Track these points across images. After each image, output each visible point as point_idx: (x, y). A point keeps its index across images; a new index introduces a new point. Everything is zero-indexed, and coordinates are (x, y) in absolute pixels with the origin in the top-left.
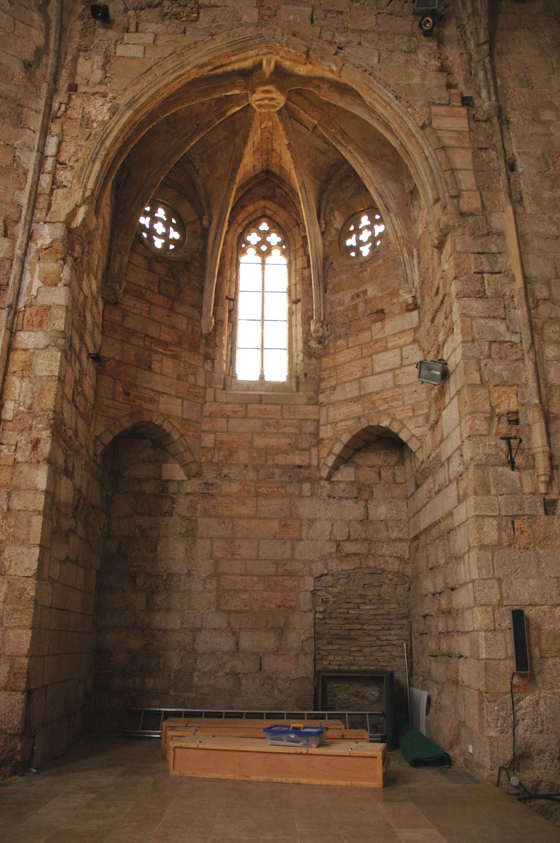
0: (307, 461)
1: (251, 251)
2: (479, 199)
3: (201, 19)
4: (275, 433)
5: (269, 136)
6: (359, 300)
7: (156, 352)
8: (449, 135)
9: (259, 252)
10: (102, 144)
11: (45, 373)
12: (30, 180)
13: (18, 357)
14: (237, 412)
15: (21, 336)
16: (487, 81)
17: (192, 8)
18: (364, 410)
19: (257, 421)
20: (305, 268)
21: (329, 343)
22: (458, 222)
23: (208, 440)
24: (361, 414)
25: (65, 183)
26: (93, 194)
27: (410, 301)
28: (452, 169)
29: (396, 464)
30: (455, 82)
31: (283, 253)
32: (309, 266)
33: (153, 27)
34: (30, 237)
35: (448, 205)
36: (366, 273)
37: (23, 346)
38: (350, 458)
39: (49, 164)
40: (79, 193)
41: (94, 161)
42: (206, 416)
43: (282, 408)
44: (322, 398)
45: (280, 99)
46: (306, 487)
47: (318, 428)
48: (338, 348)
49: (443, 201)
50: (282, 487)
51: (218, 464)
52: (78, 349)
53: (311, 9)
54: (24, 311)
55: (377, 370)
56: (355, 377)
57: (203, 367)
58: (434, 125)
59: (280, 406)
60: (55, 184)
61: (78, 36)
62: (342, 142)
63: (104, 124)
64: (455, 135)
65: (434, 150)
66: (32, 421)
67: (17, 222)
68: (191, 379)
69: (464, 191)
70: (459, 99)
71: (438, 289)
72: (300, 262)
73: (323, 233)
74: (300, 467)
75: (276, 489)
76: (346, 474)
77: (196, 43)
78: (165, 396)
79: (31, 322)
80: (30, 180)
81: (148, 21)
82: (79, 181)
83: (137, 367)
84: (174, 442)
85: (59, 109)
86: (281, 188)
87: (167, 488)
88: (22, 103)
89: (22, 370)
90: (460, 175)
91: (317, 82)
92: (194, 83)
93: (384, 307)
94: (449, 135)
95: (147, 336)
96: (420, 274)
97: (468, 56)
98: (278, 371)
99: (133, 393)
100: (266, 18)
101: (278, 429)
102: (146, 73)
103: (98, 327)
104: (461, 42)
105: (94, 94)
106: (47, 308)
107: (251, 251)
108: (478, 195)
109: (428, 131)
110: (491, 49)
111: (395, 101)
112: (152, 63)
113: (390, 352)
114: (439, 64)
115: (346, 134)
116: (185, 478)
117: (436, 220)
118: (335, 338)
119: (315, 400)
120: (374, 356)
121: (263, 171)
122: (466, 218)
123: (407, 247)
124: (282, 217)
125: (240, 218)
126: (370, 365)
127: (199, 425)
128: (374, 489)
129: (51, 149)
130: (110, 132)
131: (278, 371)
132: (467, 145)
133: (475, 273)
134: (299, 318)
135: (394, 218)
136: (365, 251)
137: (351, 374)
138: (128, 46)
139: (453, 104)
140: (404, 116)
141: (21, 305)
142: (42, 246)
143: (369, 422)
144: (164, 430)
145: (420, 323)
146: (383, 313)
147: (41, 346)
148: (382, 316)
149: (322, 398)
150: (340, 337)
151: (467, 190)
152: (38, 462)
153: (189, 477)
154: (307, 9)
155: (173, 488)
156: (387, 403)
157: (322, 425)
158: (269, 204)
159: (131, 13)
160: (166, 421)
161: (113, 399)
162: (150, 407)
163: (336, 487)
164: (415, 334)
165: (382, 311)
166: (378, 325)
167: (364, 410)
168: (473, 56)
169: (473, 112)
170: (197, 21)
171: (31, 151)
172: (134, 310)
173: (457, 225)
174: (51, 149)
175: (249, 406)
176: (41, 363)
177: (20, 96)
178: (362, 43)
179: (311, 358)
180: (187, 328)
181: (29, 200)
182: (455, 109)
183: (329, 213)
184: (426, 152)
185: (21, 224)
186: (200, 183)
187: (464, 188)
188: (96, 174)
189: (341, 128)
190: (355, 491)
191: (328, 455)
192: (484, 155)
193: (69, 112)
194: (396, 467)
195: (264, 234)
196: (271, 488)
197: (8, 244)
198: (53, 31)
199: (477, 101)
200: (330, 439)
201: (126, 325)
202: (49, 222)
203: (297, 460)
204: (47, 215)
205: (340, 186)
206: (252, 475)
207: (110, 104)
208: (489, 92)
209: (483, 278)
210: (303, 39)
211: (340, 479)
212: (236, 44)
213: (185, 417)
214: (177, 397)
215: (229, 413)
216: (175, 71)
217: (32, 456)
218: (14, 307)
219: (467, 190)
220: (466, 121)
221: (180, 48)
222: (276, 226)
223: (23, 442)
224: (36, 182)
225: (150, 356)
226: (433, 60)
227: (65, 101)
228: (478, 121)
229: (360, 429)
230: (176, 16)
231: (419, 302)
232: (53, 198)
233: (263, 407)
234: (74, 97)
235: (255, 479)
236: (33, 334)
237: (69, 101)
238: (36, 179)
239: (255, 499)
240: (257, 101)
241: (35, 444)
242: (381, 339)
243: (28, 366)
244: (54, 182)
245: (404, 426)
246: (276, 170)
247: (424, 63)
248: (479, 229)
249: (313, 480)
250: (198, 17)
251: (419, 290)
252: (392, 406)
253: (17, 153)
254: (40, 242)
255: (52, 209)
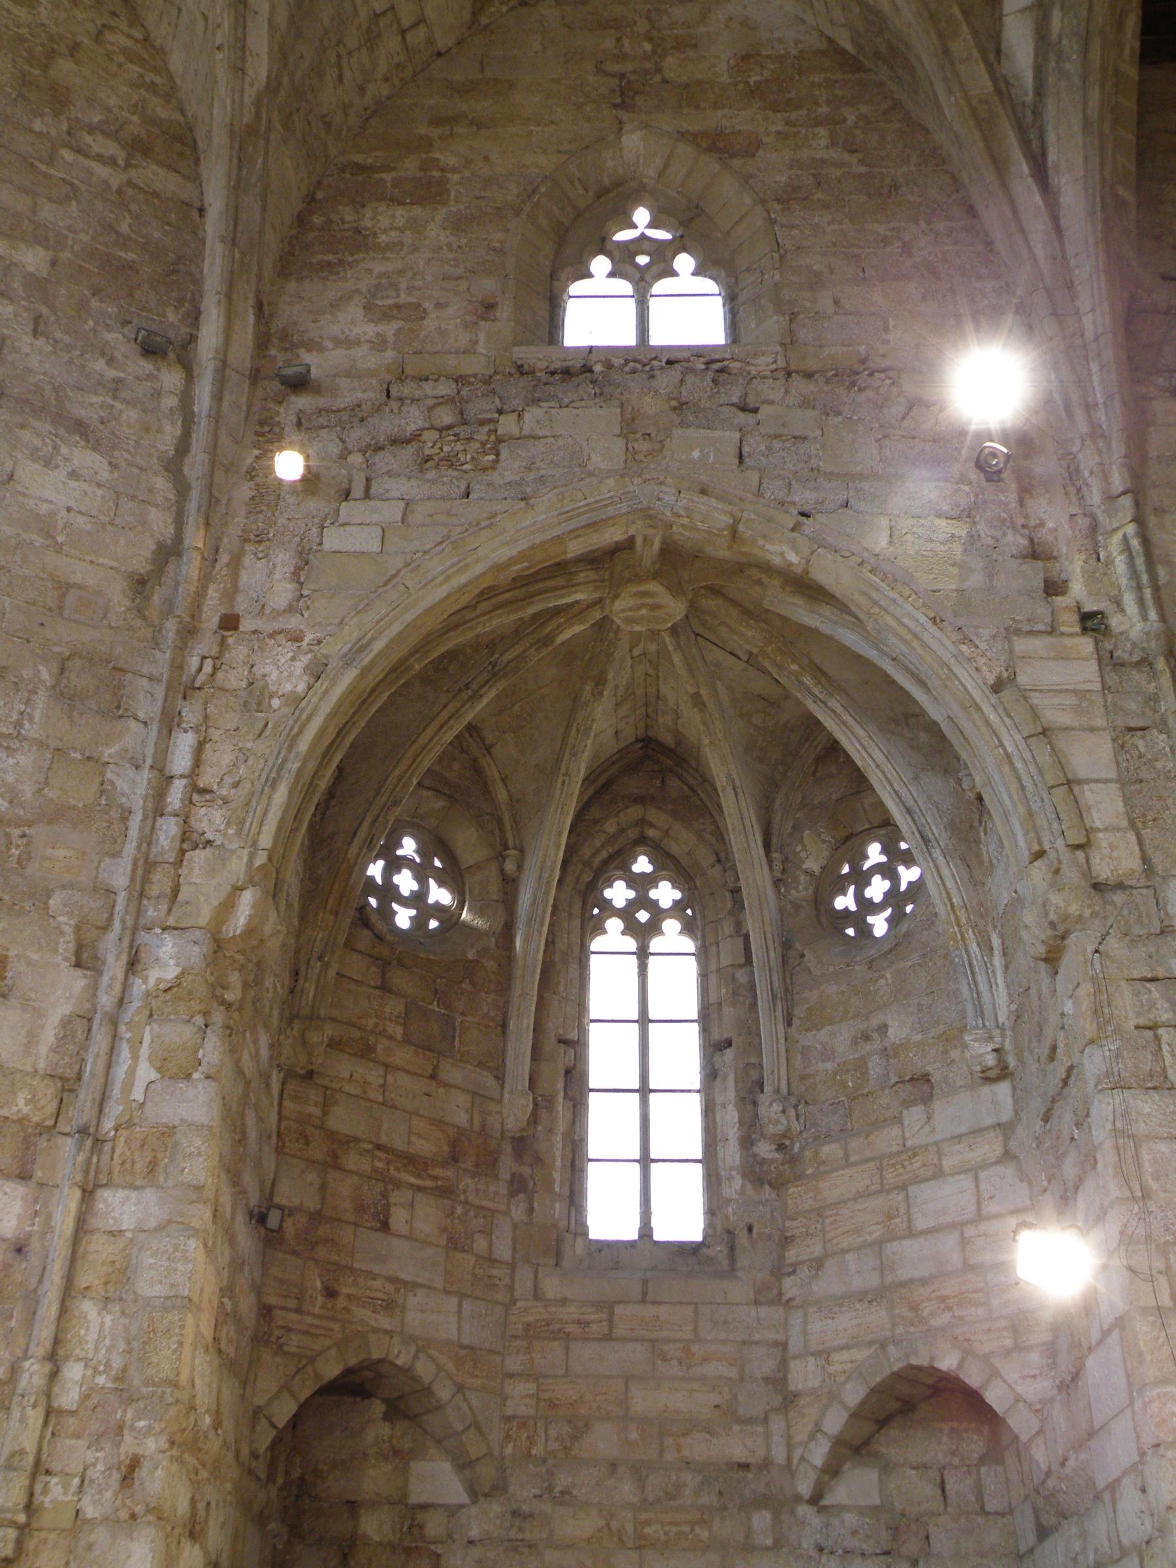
0: (761, 1453)
1: (614, 925)
2: (1137, 848)
3: (502, 464)
4: (682, 1378)
5: (651, 671)
6: (868, 1047)
7: (398, 1184)
8: (1056, 701)
9: (632, 928)
10: (291, 747)
11: (158, 1290)
12: (134, 832)
13: (100, 1249)
14: (587, 1323)
15: (105, 1201)
16: (1134, 574)
17: (483, 444)
18: (894, 1325)
19: (638, 1347)
20: (741, 966)
21: (802, 1149)
22: (1090, 906)
23: (520, 1397)
24: (888, 1333)
25: (209, 836)
26: (270, 859)
27: (991, 1060)
28: (1069, 783)
29: (982, 1460)
30: (1063, 576)
31: (688, 928)
32: (749, 960)
33: (400, 487)
34: (133, 964)
35: (1065, 867)
36: (882, 982)
37: (110, 1224)
38: (867, 1442)
39: (176, 795)
40: (240, 858)
41: (274, 786)
42: (516, 1337)
43: (696, 1312)
44: (791, 1287)
45: (676, 608)
46: (762, 1520)
47: (784, 1364)
48: (824, 1162)
49: (1052, 855)
50: (702, 1522)
51: (544, 1461)
52: (228, 1215)
53: (737, 435)
54: (114, 1139)
55: (921, 1223)
56: (870, 1239)
57: (507, 1213)
58: (1022, 679)
59: (691, 1308)
60: (189, 840)
61: (243, 512)
62: (816, 691)
63: (295, 700)
64: (1071, 700)
65: (1026, 739)
66: (125, 1411)
67: (106, 927)
68: (480, 1244)
69: (1099, 830)
70: (1075, 617)
71: (1054, 1048)
72: (729, 953)
73: (777, 882)
74: (744, 1466)
75: (687, 1528)
76: (858, 1486)
77: (493, 515)
78: (420, 1292)
79: (128, 1166)
80: (134, 832)
81: (390, 474)
82: (239, 831)
83: (356, 1224)
84: (439, 1407)
85: (200, 669)
86: (679, 777)
87: (421, 1527)
88: (121, 664)
89: (106, 1283)
90: (1088, 795)
91: (755, 574)
92: (488, 593)
93: (929, 1069)
94: (1056, 701)
95: (379, 1147)
96: (1009, 995)
97: (1088, 520)
98: (682, 1217)
99: (344, 1290)
100: (639, 457)
101: (689, 1367)
102: (386, 584)
103: (270, 1137)
104: (1072, 490)
105: (272, 635)
106: (168, 1132)
107: (614, 925)
108: (1133, 839)
109: (1008, 695)
110: (1137, 504)
111: (932, 629)
112: (399, 562)
113: (951, 1179)
114: (1025, 542)
115: (824, 673)
116: (464, 1498)
117: (1040, 901)
118: (816, 1138)
119: (775, 1292)
120: (912, 1190)
121: (637, 740)
122: (1109, 895)
123: (975, 927)
124: (682, 840)
125: (586, 852)
126: (902, 1211)
127: (498, 1359)
128: (932, 1530)
129: (181, 762)
130: (309, 718)
131: (682, 1217)
132: (1100, 722)
133: (1137, 1027)
134: (728, 1092)
135: (941, 861)
136: (879, 924)
137: (858, 1231)
138: (347, 528)
139: (1063, 629)
140: (952, 662)
141: (108, 1124)
142: (157, 985)
143: (908, 1357)
144: (417, 1379)
145: (1016, 1112)
146: (929, 1081)
147: (152, 1223)
148: (926, 1087)
149: (791, 1287)
150: (828, 1137)
151: (1106, 829)
152: (133, 1516)
153: (475, 1494)
154: (728, 433)
155: (434, 1525)
156: (950, 1309)
157: (795, 1357)
158: (653, 815)
159: (356, 459)
160: (422, 1356)
161: (298, 1311)
162: (384, 1322)
163: (835, 1522)
164: (1007, 1139)
165: (926, 1078)
166: (914, 1115)
167: (894, 1325)
168: (1101, 519)
169: (1108, 645)
170: (493, 468)
171: (137, 767)
172: (348, 1088)
173: (1087, 913)
174: (181, 762)
175: (619, 1310)
176: (151, 1267)
177: (119, 650)
178: (852, 502)
179: (762, 1184)
180: (471, 1120)
181: (133, 879)
182: (1068, 641)
183: (791, 835)
184: (1006, 743)
185: (112, 936)
186: (497, 775)
187: (1098, 824)
188: (279, 814)
189: (811, 662)
190: (884, 1534)
191: (812, 1436)
192: (1141, 744)
193: (220, 675)
194: (983, 1469)
195: (642, 884)
196: (676, 1524)
197: (83, 983)
198: (192, 506)
199: (1115, 622)
200: (814, 1393)
201: (333, 1123)
202: (175, 929)
203: (737, 1450)
204: (170, 910)
205: (815, 771)
206: (627, 1490)
207: (309, 656)
208: (1141, 601)
209: (1157, 1038)
210: (720, 498)
211: (846, 1502)
212: (579, 515)
213: (466, 1341)
214: (447, 1292)
215: (571, 1328)
216: (448, 579)
217: (118, 1502)
218: (92, 1130)
219: (1106, 829)
220: (1093, 665)
221: (459, 529)
222: (670, 865)
223: (100, 1467)
224: (148, 839)
225: (385, 1196)
226: (1010, 532)
227: (213, 653)
228: (1123, 665)
229: (887, 1372)
230: (450, 461)
231: (1012, 1061)
232: (183, 871)
233: (650, 1311)
234: (230, 641)
235: (635, 1500)
236: (134, 1194)
237: (221, 652)
238: (147, 831)
239: (635, 1555)
240: (623, 611)
241: (130, 1470)
242: (926, 1147)
243: (122, 1275)
244: (185, 836)
245: (995, 1374)
246: (669, 741)
247: (991, 542)
248: (1139, 920)
249: (779, 1504)
250: (497, 461)
251: (1008, 1033)
252: (961, 1318)
253: (109, 775)
254: (154, 975)
255: (180, 898)
